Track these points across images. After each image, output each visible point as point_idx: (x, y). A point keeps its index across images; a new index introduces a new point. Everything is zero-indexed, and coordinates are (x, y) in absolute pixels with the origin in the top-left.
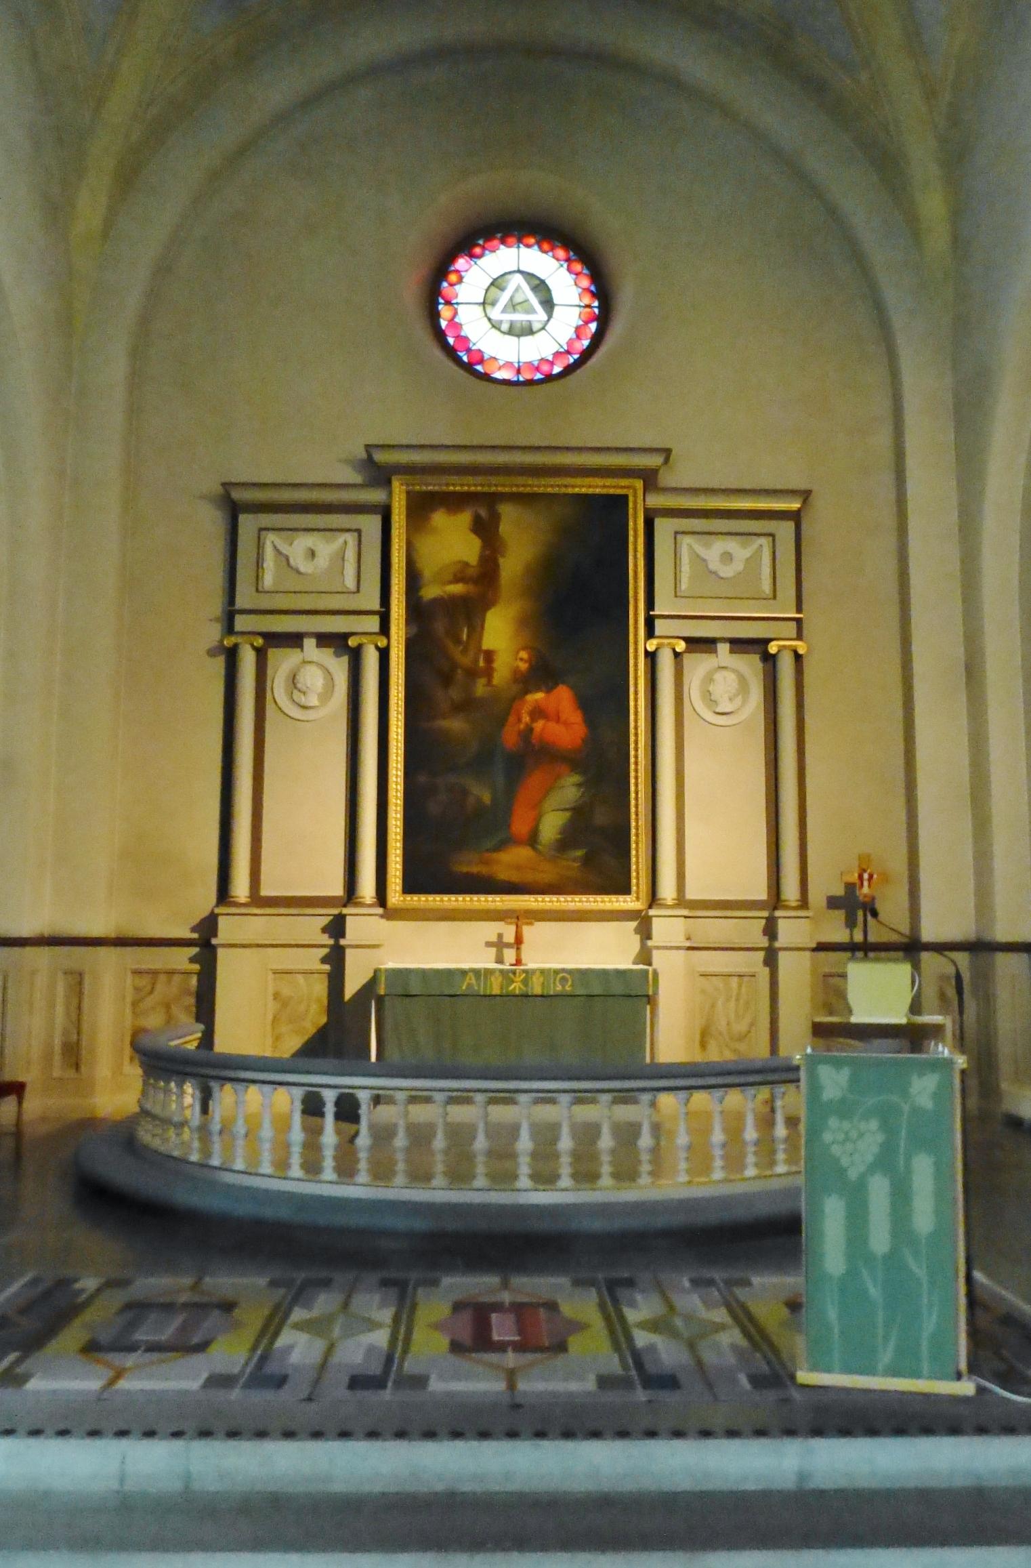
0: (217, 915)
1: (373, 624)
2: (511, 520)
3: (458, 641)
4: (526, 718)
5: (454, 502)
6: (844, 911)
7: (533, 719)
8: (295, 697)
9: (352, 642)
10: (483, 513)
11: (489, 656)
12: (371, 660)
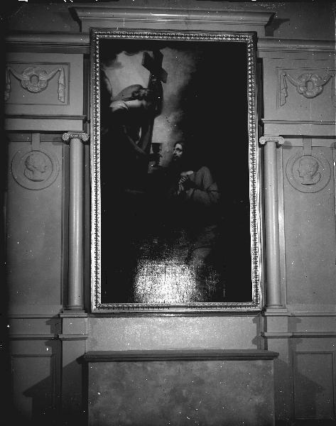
0: (62, 318)
1: (78, 125)
2: (169, 61)
3: (136, 138)
4: (181, 188)
5: (132, 47)
6: (114, 110)
7: (186, 189)
8: (28, 175)
9: (66, 137)
10: (151, 53)
11: (157, 146)
12: (77, 146)
